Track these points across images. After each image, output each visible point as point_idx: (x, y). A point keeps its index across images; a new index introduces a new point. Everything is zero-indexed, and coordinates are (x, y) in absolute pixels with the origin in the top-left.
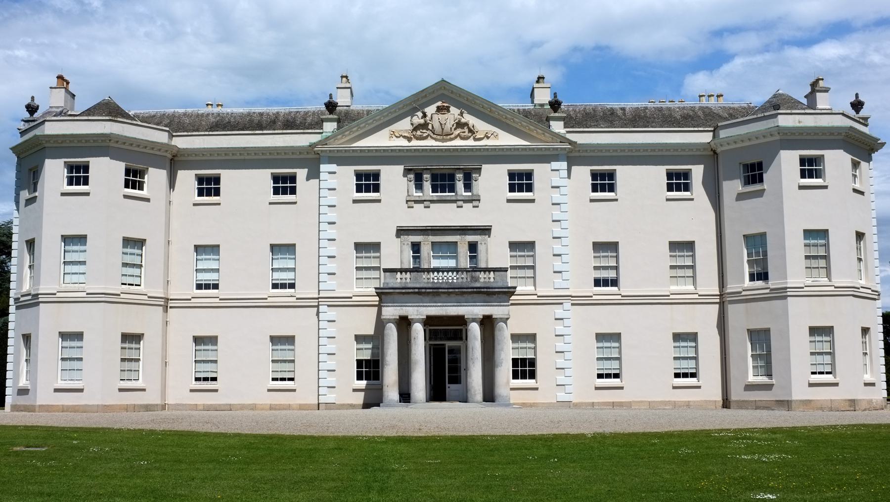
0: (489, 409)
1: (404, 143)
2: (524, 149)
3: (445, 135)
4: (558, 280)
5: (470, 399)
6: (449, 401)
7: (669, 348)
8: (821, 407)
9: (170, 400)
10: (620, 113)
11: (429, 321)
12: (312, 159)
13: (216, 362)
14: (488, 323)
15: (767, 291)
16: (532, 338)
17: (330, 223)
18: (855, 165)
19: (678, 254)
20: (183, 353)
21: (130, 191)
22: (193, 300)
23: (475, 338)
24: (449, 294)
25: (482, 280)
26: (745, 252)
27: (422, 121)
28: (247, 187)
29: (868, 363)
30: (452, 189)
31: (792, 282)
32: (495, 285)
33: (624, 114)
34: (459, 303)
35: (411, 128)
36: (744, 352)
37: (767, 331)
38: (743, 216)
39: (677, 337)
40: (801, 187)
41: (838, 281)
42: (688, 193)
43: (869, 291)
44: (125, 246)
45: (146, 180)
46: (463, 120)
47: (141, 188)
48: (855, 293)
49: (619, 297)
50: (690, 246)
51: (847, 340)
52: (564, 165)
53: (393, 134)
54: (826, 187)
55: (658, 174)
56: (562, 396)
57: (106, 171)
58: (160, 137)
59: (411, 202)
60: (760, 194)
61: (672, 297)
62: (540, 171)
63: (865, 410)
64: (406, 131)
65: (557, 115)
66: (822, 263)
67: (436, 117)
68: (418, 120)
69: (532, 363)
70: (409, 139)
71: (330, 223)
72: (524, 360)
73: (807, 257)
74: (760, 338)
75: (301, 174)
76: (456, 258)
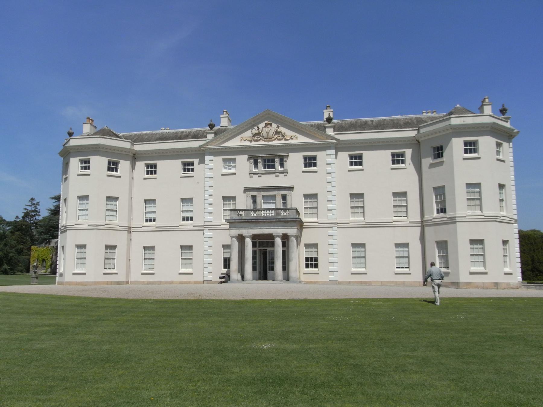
0: (286, 285)
1: (247, 143)
2: (311, 144)
3: (269, 139)
4: (330, 215)
5: (275, 279)
6: (270, 280)
7: (394, 252)
8: (477, 286)
9: (132, 279)
10: (370, 123)
11: (254, 237)
12: (201, 154)
13: (192, 259)
14: (285, 238)
15: (446, 219)
16: (316, 246)
17: (210, 187)
18: (499, 145)
19: (397, 199)
20: (138, 253)
21: (111, 173)
22: (143, 228)
23: (279, 246)
24: (264, 222)
25: (282, 214)
26: (434, 197)
27: (257, 132)
28: (170, 168)
29: (508, 261)
30: (273, 167)
31: (459, 213)
32: (289, 217)
33: (372, 124)
34: (269, 227)
35: (252, 135)
36: (435, 255)
37: (446, 242)
38: (433, 177)
39: (398, 245)
40: (465, 159)
41: (487, 212)
42: (403, 165)
43: (508, 219)
44: (107, 200)
45: (119, 167)
46: (279, 130)
47: (116, 171)
48: (498, 220)
49: (364, 223)
50: (404, 194)
51: (493, 247)
52: (333, 152)
53: (242, 139)
54: (479, 158)
55: (386, 155)
56: (332, 278)
57: (99, 163)
58: (126, 145)
59: (252, 174)
60: (441, 164)
61: (394, 223)
62: (320, 156)
63: (505, 289)
64: (249, 137)
65: (330, 125)
66: (478, 202)
67: (264, 129)
68: (255, 131)
69: (316, 259)
70: (251, 141)
71: (210, 187)
72: (312, 258)
73: (468, 199)
74: (442, 245)
75: (196, 161)
76: (275, 203)
